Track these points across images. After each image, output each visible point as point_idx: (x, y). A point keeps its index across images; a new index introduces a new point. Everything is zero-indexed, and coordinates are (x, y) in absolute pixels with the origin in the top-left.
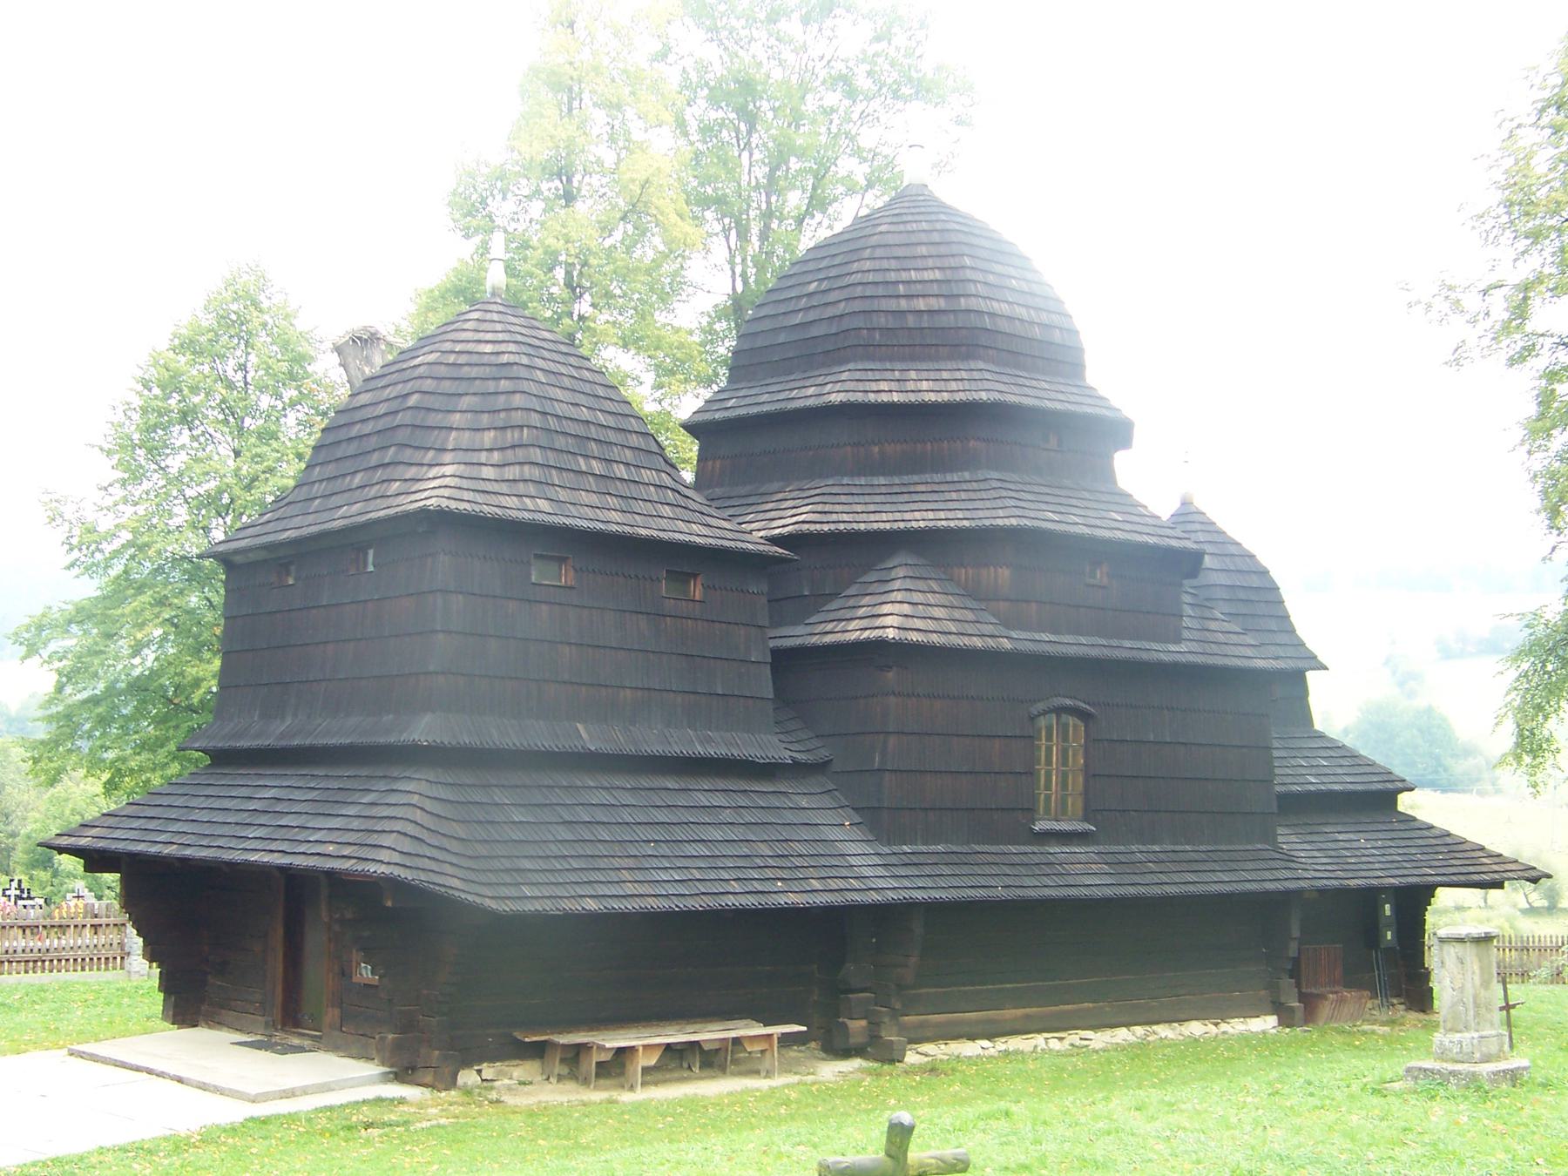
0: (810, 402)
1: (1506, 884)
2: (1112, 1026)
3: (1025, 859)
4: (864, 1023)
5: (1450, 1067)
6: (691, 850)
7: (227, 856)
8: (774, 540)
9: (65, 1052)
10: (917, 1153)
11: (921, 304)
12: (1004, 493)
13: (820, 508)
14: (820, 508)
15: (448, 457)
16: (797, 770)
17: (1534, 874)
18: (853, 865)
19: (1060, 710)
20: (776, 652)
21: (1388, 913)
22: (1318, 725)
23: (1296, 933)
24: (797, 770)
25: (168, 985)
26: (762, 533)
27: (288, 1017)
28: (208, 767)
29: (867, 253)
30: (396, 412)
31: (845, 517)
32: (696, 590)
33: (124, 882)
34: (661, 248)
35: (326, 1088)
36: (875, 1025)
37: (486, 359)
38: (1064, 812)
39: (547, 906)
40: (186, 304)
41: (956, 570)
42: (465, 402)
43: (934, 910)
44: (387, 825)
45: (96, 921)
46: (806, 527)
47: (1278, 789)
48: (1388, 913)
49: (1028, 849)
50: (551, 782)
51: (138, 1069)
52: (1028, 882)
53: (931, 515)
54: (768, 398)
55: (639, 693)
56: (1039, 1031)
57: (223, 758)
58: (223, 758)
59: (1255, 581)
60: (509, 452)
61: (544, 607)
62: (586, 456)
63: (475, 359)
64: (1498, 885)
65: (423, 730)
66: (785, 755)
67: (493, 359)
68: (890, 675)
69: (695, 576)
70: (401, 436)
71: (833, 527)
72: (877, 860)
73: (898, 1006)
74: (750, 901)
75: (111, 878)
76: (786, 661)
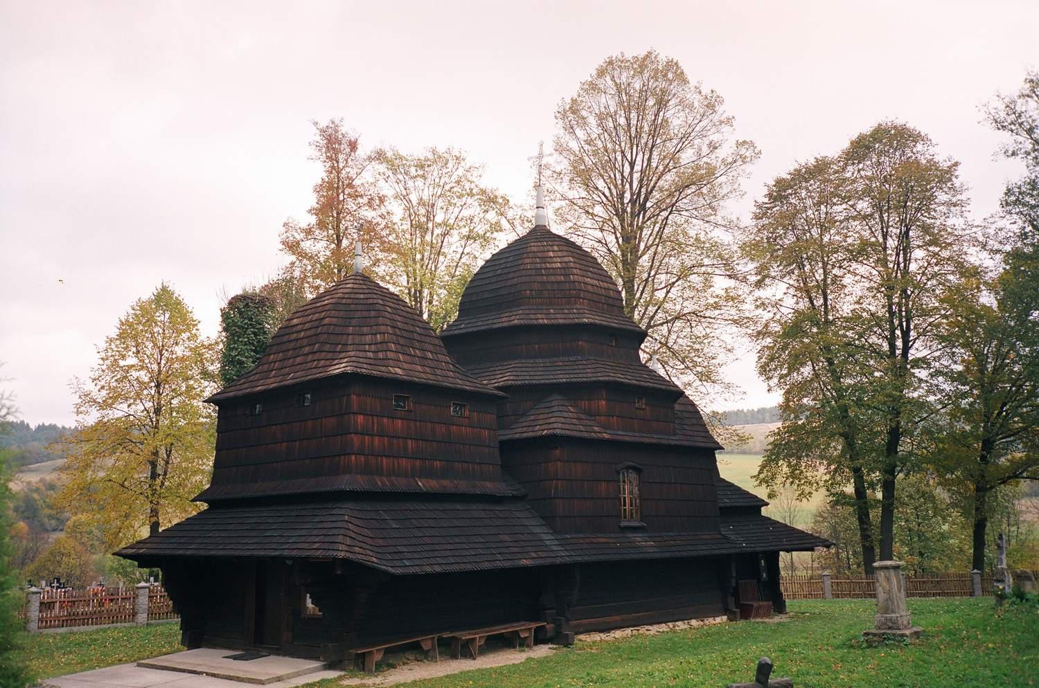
0: (506, 324)
2: (659, 623)
4: (552, 625)
5: (882, 631)
6: (475, 539)
7: (237, 553)
8: (498, 388)
9: (135, 664)
10: (773, 679)
11: (553, 279)
12: (598, 366)
13: (515, 373)
14: (515, 373)
15: (350, 348)
16: (514, 499)
18: (547, 547)
19: (629, 468)
20: (501, 443)
21: (763, 564)
22: (722, 476)
23: (734, 575)
24: (514, 499)
25: (185, 627)
27: (256, 642)
29: (525, 255)
30: (318, 327)
31: (528, 378)
35: (298, 674)
36: (559, 626)
37: (361, 302)
38: (632, 517)
39: (417, 570)
41: (579, 402)
42: (354, 322)
43: (587, 567)
44: (336, 532)
45: (112, 597)
46: (510, 382)
48: (763, 564)
50: (405, 508)
51: (183, 671)
53: (567, 376)
54: (482, 323)
55: (443, 463)
56: (628, 627)
59: (690, 408)
60: (379, 346)
61: (400, 421)
62: (413, 348)
63: (356, 301)
65: (345, 482)
66: (509, 493)
67: (365, 301)
68: (558, 451)
70: (323, 338)
71: (523, 382)
72: (557, 542)
73: (568, 616)
74: (507, 564)
76: (508, 447)
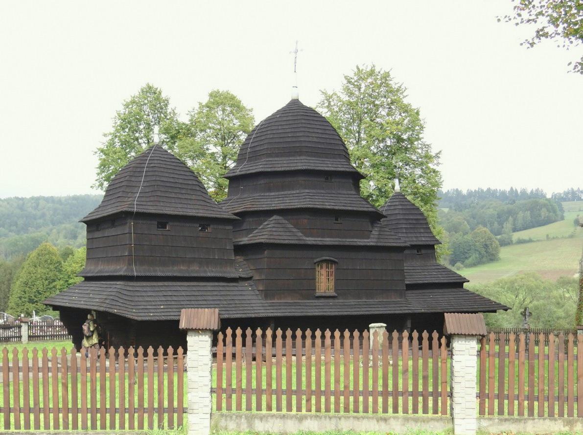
1: (497, 311)
3: (311, 304)
8: (236, 214)
10: (366, 330)
17: (506, 308)
26: (231, 212)
28: (84, 281)
32: (209, 230)
33: (60, 313)
34: (175, 150)
40: (133, 90)
47: (406, 282)
49: (313, 301)
52: (309, 311)
57: (88, 279)
58: (88, 279)
64: (495, 311)
69: (209, 225)
75: (58, 312)
